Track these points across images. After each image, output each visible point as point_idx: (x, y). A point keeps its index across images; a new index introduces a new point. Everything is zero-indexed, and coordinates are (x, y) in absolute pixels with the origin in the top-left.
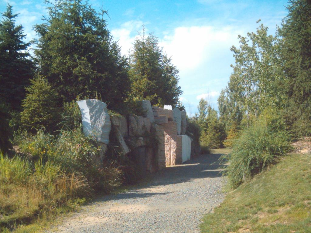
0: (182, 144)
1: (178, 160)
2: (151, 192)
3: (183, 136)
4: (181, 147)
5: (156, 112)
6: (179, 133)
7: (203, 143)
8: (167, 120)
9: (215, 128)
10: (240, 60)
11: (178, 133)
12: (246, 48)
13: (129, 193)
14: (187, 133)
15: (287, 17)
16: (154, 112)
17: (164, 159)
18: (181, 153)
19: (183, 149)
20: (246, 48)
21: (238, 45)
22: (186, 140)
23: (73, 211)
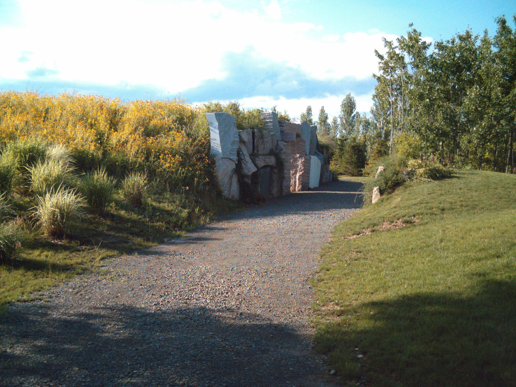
0: (310, 167)
1: (305, 186)
2: (203, 237)
3: (312, 156)
4: (309, 170)
5: (283, 126)
6: (308, 153)
7: (332, 167)
8: (295, 136)
9: (353, 147)
10: (386, 68)
11: (306, 152)
12: (393, 55)
13: (508, 159)
14: (315, 154)
15: (161, 253)
16: (280, 126)
17: (288, 183)
18: (309, 177)
19: (311, 173)
20: (393, 55)
21: (384, 51)
22: (316, 162)
23: (252, 128)
